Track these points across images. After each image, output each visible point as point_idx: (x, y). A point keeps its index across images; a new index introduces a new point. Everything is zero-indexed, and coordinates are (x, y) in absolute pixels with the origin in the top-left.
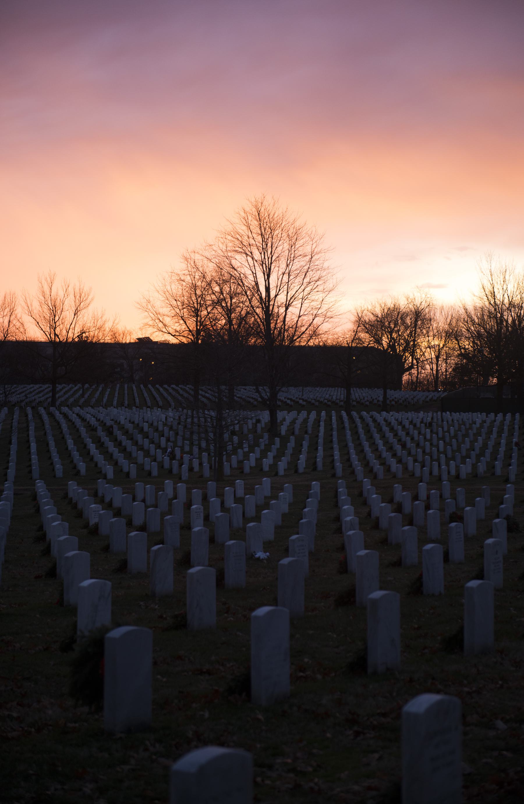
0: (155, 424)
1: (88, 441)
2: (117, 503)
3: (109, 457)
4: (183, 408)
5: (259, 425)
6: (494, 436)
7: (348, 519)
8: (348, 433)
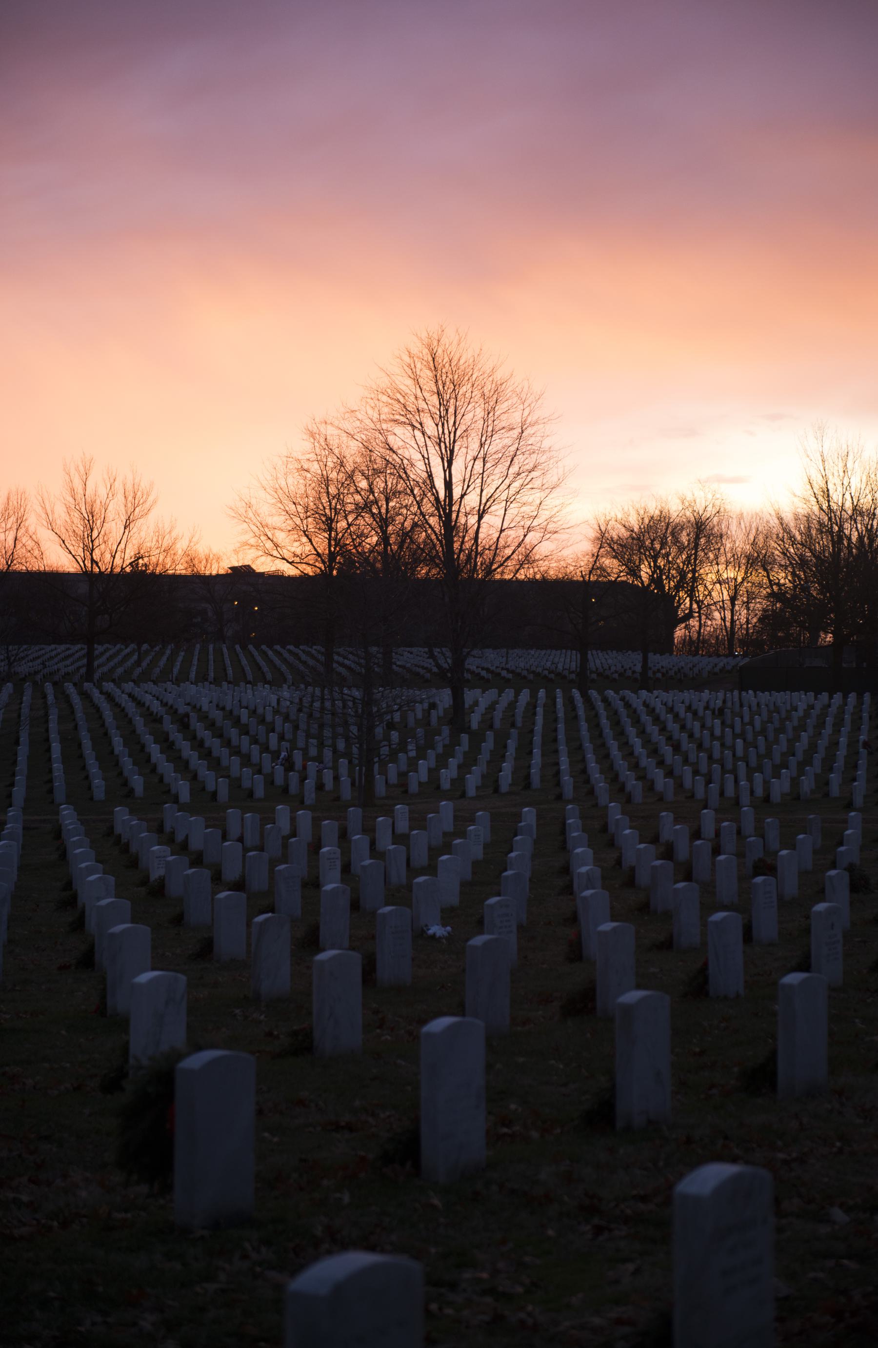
0: (260, 711)
1: (148, 739)
2: (196, 844)
3: (182, 766)
4: (307, 684)
5: (433, 713)
6: (828, 730)
7: (584, 869)
8: (584, 725)
